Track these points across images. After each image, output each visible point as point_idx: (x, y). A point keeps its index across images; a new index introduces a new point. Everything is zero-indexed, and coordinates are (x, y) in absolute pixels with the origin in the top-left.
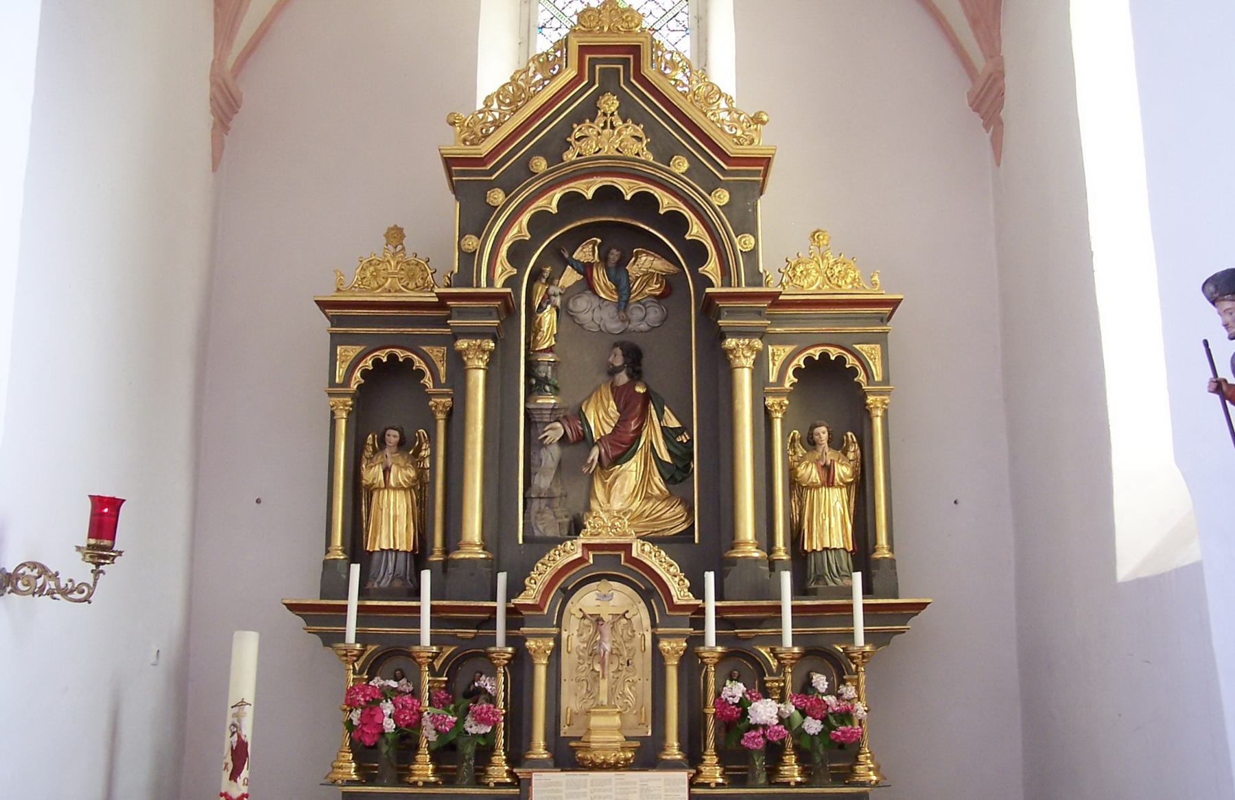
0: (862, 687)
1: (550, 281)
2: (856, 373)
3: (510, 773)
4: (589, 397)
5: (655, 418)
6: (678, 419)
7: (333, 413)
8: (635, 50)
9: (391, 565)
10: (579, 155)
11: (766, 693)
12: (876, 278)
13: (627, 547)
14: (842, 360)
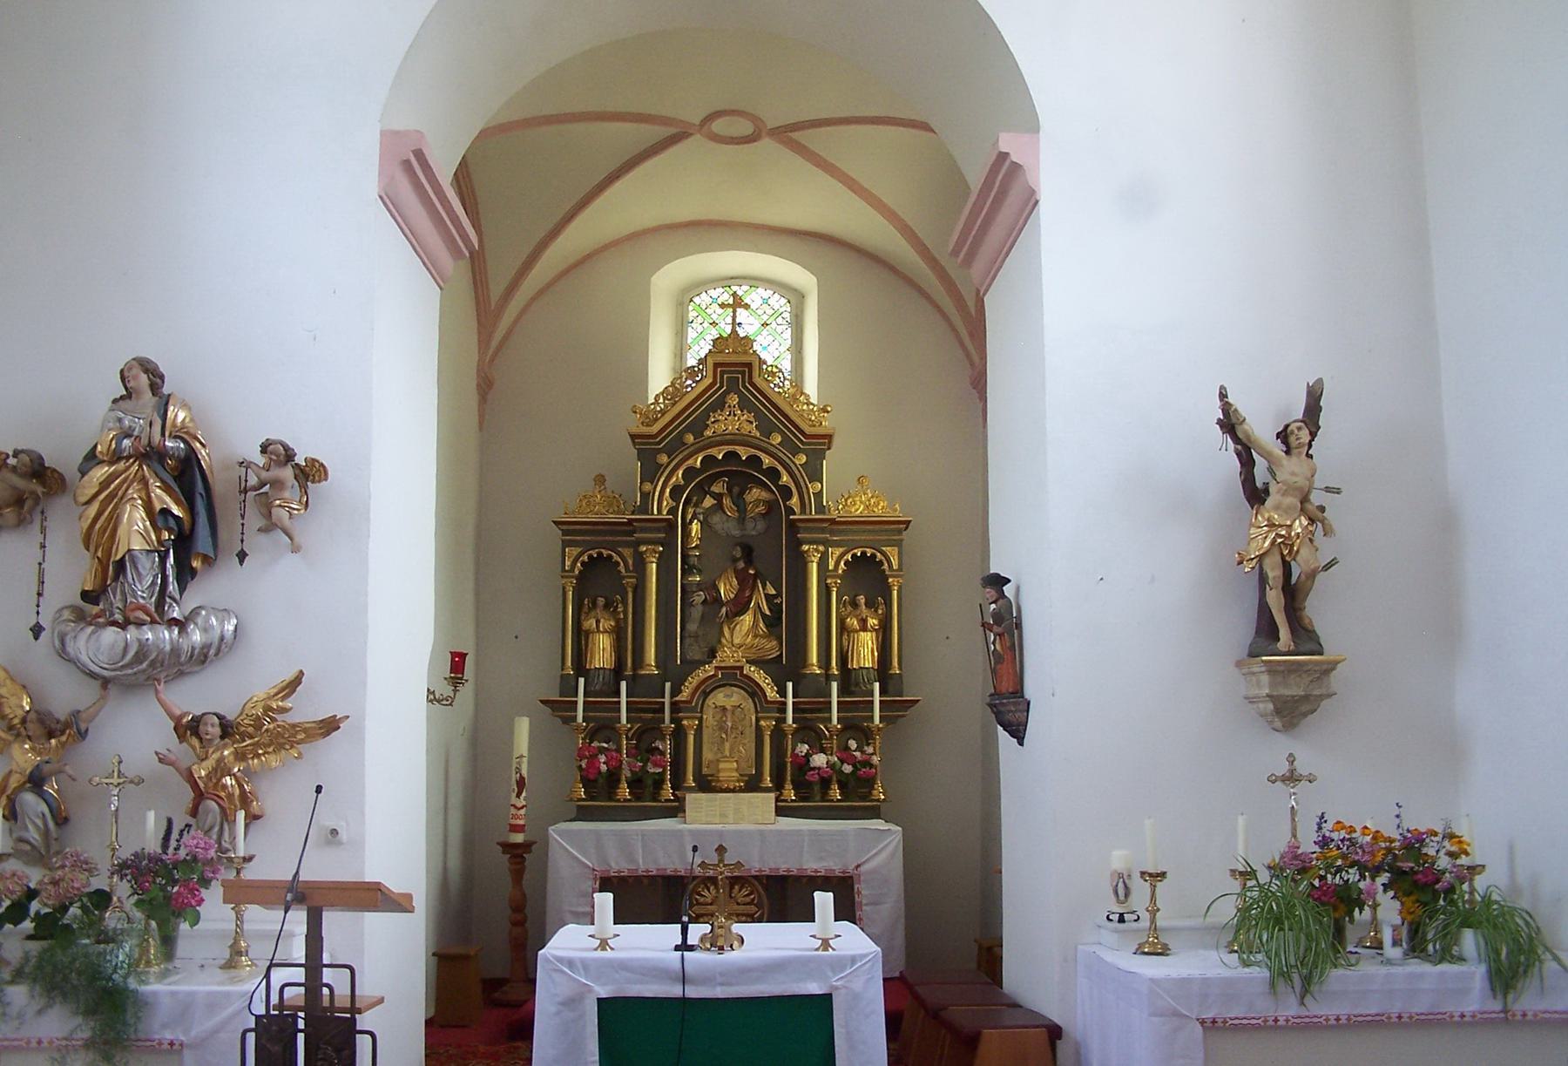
0: (877, 748)
1: (696, 505)
2: (883, 564)
3: (673, 794)
4: (721, 576)
5: (761, 589)
6: (775, 590)
7: (564, 588)
8: (749, 365)
9: (601, 677)
10: (714, 432)
11: (823, 750)
12: (897, 506)
13: (741, 668)
14: (874, 556)
